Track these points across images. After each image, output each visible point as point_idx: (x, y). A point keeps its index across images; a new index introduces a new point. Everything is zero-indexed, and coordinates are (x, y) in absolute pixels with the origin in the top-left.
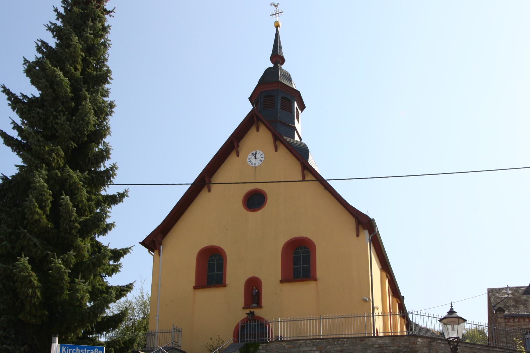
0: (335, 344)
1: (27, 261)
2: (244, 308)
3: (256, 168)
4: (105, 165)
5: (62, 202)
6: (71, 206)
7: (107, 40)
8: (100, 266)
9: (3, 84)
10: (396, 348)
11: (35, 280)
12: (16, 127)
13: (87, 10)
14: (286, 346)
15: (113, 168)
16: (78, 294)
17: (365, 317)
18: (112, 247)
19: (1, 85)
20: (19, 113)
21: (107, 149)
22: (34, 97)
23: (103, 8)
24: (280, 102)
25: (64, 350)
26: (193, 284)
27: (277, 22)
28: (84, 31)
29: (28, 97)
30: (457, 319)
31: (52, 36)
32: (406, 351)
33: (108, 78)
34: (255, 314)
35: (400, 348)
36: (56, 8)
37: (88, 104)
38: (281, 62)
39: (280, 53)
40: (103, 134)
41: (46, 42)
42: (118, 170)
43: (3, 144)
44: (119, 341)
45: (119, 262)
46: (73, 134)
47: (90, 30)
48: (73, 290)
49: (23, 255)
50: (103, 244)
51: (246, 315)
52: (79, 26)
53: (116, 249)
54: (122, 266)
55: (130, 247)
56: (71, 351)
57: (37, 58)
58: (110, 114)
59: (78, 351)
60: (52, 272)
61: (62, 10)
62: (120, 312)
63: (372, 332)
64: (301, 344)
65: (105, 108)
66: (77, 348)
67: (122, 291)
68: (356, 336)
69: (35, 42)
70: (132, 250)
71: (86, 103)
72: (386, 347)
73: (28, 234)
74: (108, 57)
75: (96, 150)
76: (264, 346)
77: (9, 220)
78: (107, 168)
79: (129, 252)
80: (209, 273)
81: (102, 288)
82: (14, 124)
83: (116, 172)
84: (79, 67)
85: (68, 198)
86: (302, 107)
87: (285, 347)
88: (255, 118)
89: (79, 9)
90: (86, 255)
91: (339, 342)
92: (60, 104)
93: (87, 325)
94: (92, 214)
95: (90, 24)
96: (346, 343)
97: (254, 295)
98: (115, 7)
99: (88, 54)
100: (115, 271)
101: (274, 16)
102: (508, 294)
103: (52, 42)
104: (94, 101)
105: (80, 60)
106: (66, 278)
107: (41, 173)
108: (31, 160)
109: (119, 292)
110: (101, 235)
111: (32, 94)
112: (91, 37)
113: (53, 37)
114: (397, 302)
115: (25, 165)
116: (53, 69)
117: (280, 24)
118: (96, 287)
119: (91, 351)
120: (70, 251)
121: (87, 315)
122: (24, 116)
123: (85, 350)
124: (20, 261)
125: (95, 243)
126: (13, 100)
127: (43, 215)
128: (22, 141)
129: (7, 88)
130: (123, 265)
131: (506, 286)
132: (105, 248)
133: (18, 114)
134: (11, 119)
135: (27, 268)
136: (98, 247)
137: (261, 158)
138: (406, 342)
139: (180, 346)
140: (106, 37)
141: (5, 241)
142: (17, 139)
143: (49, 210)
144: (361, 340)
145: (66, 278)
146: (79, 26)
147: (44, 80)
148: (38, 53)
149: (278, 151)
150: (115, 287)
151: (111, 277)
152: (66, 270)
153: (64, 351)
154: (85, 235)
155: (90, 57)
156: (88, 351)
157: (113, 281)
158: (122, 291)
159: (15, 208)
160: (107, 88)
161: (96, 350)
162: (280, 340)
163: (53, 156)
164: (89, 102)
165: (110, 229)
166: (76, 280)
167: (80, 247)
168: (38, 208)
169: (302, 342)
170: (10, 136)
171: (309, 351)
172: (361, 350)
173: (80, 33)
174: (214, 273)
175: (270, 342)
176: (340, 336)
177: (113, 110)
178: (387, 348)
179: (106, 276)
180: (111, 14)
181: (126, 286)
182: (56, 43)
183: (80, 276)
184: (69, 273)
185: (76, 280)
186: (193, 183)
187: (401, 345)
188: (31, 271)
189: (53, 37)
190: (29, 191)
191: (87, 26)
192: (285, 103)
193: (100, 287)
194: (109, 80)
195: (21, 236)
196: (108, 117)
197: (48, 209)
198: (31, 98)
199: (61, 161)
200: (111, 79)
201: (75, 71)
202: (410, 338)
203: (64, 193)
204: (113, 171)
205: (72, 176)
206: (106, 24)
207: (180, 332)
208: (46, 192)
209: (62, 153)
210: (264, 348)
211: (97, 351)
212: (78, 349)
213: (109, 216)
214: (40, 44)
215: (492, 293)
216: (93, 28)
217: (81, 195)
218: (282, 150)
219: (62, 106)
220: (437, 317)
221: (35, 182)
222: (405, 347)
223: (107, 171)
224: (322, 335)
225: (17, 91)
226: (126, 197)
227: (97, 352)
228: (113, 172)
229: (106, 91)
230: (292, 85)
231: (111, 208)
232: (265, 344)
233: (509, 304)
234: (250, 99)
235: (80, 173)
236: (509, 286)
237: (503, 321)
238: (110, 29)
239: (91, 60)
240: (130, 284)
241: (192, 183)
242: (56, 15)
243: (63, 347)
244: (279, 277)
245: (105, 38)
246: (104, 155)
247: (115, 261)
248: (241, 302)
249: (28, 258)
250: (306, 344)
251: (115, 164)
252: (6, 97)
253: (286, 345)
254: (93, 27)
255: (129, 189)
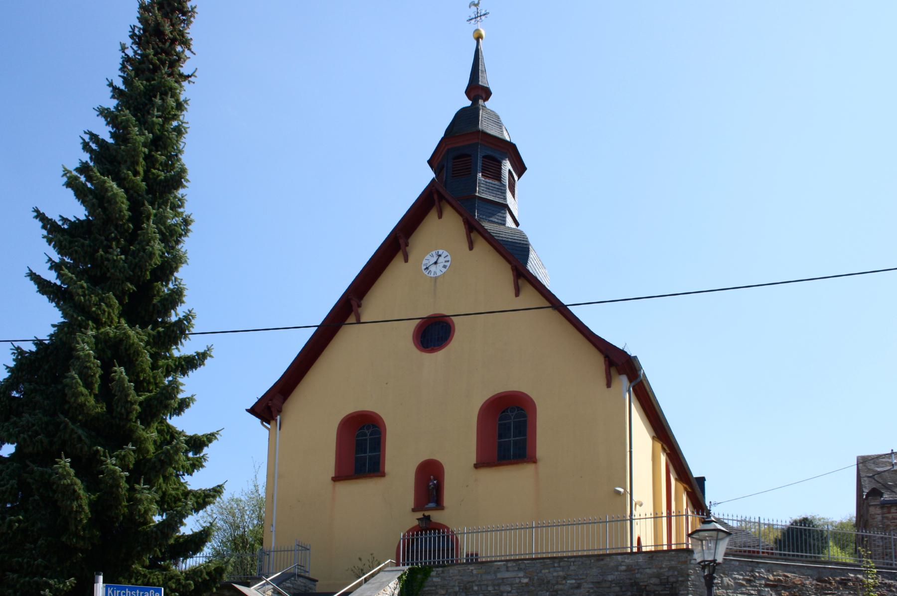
0: (554, 567)
1: (68, 464)
2: (414, 510)
3: (436, 278)
4: (178, 312)
5: (114, 376)
6: (127, 381)
7: (182, 123)
8: (170, 464)
9: (36, 207)
10: (655, 571)
11: (80, 489)
12: (55, 266)
13: (154, 80)
14: (475, 572)
15: (188, 318)
16: (140, 507)
17: (606, 522)
18: (190, 432)
19: (33, 208)
20: (57, 248)
21: (180, 289)
22: (78, 219)
23: (178, 72)
24: (481, 164)
25: (110, 592)
26: (332, 473)
27: (477, 31)
28: (149, 113)
29: (70, 221)
30: (714, 533)
31: (105, 122)
32: (672, 576)
33: (183, 180)
34: (431, 519)
35: (662, 571)
36: (110, 81)
37: (151, 226)
38: (484, 97)
39: (482, 82)
40: (174, 267)
41: (96, 135)
42: (195, 319)
43: (37, 292)
44: (201, 571)
45: (201, 455)
46: (131, 273)
47: (158, 111)
48: (134, 501)
49: (63, 456)
50: (177, 429)
51: (417, 521)
52: (141, 107)
53: (196, 435)
54: (207, 459)
55: (217, 431)
56: (120, 593)
57: (82, 162)
58: (186, 233)
59: (128, 593)
60: (104, 477)
61: (119, 83)
62: (202, 529)
63: (629, 546)
64: (498, 568)
65: (177, 227)
66: (127, 590)
67: (204, 499)
68: (591, 553)
69: (80, 136)
70: (221, 436)
71: (148, 225)
72: (638, 569)
73: (70, 424)
74: (184, 147)
75: (164, 291)
76: (439, 571)
77: (46, 403)
78: (180, 318)
79: (216, 438)
80: (357, 456)
81: (176, 494)
82: (50, 262)
83: (193, 322)
84: (141, 169)
85: (122, 369)
86: (520, 168)
87: (472, 573)
88: (436, 197)
89: (142, 81)
90: (151, 450)
91: (562, 564)
92: (113, 229)
93: (155, 549)
94: (158, 389)
95: (158, 101)
96: (574, 565)
97: (431, 488)
98: (196, 69)
99: (154, 148)
100: (197, 467)
101: (473, 21)
102: (893, 465)
103: (105, 132)
104: (160, 220)
105: (141, 160)
106: (124, 484)
107: (86, 334)
108: (72, 316)
109: (202, 499)
110: (175, 416)
111: (75, 217)
112: (159, 121)
113: (106, 125)
114: (686, 489)
115: (66, 321)
116: (103, 179)
117: (483, 33)
118: (169, 493)
119: (146, 593)
120: (127, 445)
121: (154, 535)
122: (63, 252)
123: (138, 592)
124: (60, 464)
125: (165, 428)
126: (50, 228)
127: (90, 395)
128: (62, 285)
129: (41, 212)
130: (208, 458)
131: (890, 452)
132: (181, 433)
133: (56, 250)
134: (47, 255)
135: (68, 474)
136: (171, 434)
137: (446, 262)
138: (673, 560)
139: (308, 572)
140: (181, 118)
141: (40, 435)
142: (55, 284)
143: (98, 387)
144: (598, 560)
145: (124, 484)
146: (141, 107)
147: (91, 197)
148: (84, 151)
149: (475, 249)
150: (196, 492)
151: (191, 477)
152: (122, 473)
153: (110, 594)
154: (149, 420)
155: (157, 151)
156: (141, 593)
157: (196, 482)
158: (204, 499)
159: (53, 385)
160: (182, 195)
161: (152, 592)
162: (473, 559)
163: (102, 308)
164: (153, 223)
165: (188, 406)
166: (137, 486)
167: (143, 439)
168: (83, 386)
169: (501, 565)
170: (46, 281)
171: (511, 578)
172: (597, 575)
173: (143, 116)
174: (366, 455)
175: (449, 566)
176: (565, 555)
177: (189, 227)
178: (640, 570)
179: (184, 475)
180: (190, 79)
181: (212, 489)
182: (110, 132)
183: (142, 481)
184: (127, 477)
185: (137, 486)
186: (321, 324)
187: (664, 566)
188: (74, 478)
189: (106, 125)
190: (71, 361)
191: (153, 106)
192: (493, 167)
193: (173, 492)
194: (185, 183)
195: (62, 426)
196: (182, 238)
197: (96, 386)
198: (75, 221)
199: (114, 314)
200: (187, 181)
201: (135, 175)
202: (680, 555)
203: (116, 364)
204: (189, 321)
205: (129, 336)
206: (182, 98)
207: (308, 549)
208: (93, 363)
209: (115, 302)
210: (439, 574)
211: (153, 594)
212: (129, 590)
213: (182, 391)
214: (87, 138)
215: (864, 463)
216: (163, 108)
217: (142, 362)
218: (482, 246)
219: (116, 232)
220: (734, 519)
221: (78, 351)
222: (671, 568)
223: (180, 321)
224: (534, 554)
225: (53, 215)
226: (208, 358)
227: (153, 595)
228: (189, 323)
229: (179, 200)
230: (502, 134)
231: (188, 375)
232: (440, 569)
233: (891, 482)
234: (431, 162)
235: (140, 329)
236: (894, 451)
237: (879, 511)
238: (187, 104)
239: (158, 156)
240: (219, 486)
241: (319, 324)
242: (111, 92)
243: (109, 588)
244: (474, 460)
245: (180, 120)
246: (176, 297)
247: (195, 454)
248: (409, 498)
249: (69, 460)
250: (507, 567)
251: (192, 311)
252: (41, 224)
253: (475, 569)
254: (162, 105)
255: (212, 345)
